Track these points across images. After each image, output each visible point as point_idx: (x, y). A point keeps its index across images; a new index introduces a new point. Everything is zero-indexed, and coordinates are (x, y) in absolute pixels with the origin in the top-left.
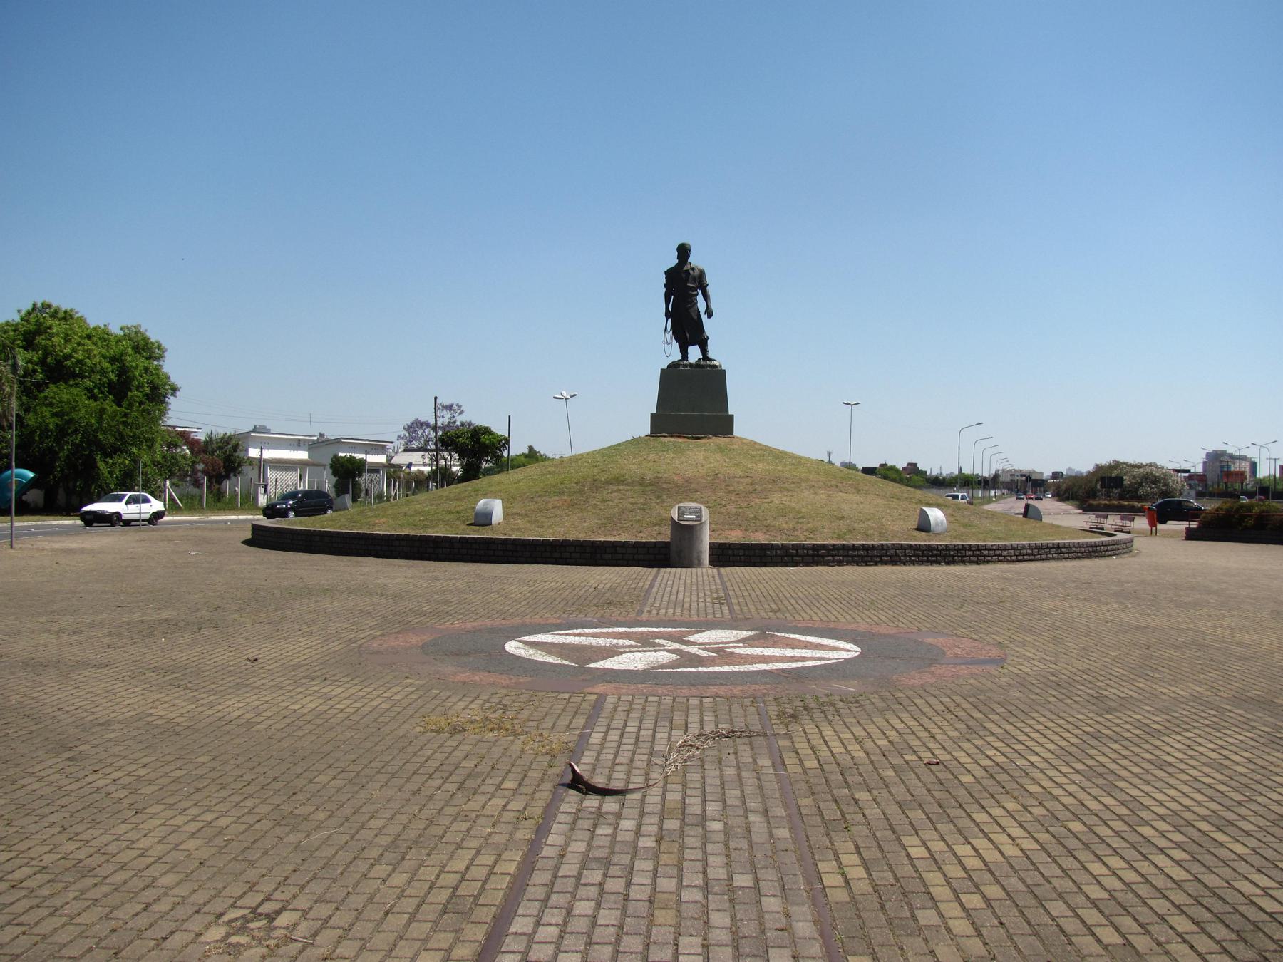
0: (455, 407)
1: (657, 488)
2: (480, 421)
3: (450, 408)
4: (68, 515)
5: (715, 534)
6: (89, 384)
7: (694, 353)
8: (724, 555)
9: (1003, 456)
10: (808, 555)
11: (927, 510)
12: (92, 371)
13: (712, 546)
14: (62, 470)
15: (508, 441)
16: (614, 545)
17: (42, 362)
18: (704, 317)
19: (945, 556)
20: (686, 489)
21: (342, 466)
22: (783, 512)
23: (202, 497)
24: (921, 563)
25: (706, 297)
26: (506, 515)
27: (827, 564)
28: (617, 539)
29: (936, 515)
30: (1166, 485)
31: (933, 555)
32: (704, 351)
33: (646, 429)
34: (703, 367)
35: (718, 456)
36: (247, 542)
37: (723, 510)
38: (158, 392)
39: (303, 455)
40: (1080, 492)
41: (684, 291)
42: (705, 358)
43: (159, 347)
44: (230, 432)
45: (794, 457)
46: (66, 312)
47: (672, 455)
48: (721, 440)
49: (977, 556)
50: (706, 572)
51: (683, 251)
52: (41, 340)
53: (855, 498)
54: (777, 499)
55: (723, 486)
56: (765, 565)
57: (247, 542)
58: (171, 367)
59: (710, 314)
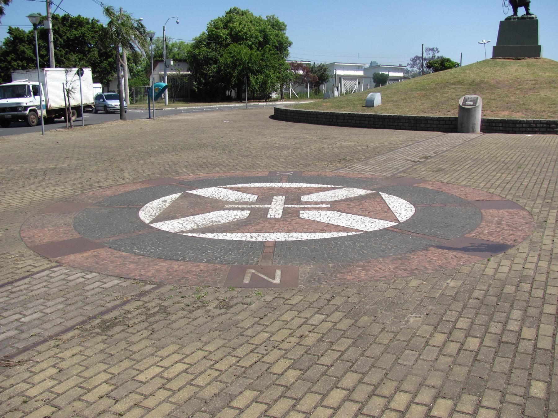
0: (435, 49)
2: (446, 56)
3: (432, 50)
4: (241, 102)
6: (250, 43)
7: (521, 11)
10: (543, 127)
12: (251, 37)
13: (483, 121)
14: (235, 81)
17: (230, 34)
28: (432, 115)
32: (527, 9)
33: (490, 55)
34: (525, 18)
36: (272, 117)
38: (282, 47)
39: (361, 73)
42: (528, 13)
44: (323, 63)
46: (242, 12)
52: (231, 25)
57: (272, 117)
58: (289, 34)
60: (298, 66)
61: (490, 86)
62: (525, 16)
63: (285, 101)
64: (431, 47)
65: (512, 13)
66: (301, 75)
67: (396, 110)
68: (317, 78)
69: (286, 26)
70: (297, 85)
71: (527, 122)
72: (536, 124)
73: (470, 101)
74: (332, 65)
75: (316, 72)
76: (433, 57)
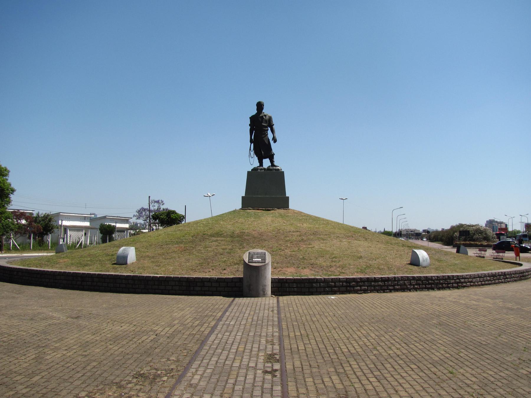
0: (160, 202)
1: (242, 239)
2: (171, 208)
3: (158, 202)
5: (276, 271)
7: (266, 163)
8: (282, 288)
9: (407, 223)
10: (342, 286)
11: (415, 250)
13: (274, 281)
15: (184, 217)
16: (203, 281)
18: (272, 142)
19: (437, 284)
20: (259, 239)
21: (105, 229)
22: (322, 254)
23: (30, 244)
24: (421, 289)
25: (273, 131)
26: (139, 256)
27: (356, 292)
29: (422, 254)
30: (486, 234)
31: (429, 284)
32: (272, 161)
33: (239, 206)
34: (271, 170)
35: (280, 219)
37: (282, 253)
39: (87, 224)
40: (444, 238)
41: (260, 129)
42: (273, 165)
43: (6, 170)
45: (323, 220)
47: (253, 219)
48: (282, 211)
49: (458, 283)
50: (270, 301)
51: (260, 106)
53: (366, 244)
54: (317, 245)
55: (282, 237)
56: (311, 293)
59: (275, 141)
60: (20, 215)
61: (254, 238)
62: (271, 168)
63: (5, 253)
64: (156, 200)
65: (258, 164)
66: (24, 225)
67: (157, 268)
68: (42, 228)
69: (9, 172)
70: (19, 235)
71: (325, 281)
72: (335, 283)
73: (258, 258)
74: (58, 215)
75: (40, 221)
76: (159, 209)
